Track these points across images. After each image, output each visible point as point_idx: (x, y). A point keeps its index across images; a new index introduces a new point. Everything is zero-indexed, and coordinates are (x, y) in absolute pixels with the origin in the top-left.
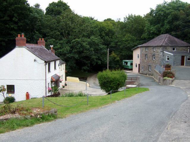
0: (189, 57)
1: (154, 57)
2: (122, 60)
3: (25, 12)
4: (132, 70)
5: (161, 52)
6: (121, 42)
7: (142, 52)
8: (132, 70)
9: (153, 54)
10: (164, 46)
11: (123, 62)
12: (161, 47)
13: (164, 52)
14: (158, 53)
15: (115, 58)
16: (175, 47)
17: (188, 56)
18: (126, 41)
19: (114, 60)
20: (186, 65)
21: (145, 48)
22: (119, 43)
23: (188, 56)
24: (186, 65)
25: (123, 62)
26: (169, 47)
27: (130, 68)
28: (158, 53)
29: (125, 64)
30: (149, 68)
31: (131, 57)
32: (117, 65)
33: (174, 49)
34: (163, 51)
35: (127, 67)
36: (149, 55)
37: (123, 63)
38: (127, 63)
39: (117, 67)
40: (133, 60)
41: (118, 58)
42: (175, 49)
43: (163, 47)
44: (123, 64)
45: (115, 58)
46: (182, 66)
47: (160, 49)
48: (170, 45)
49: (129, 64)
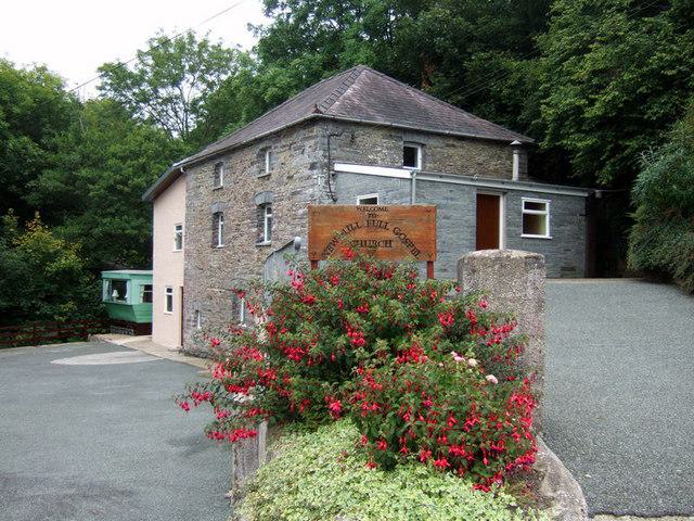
0: (529, 205)
1: (269, 219)
2: (96, 270)
3: (564, 472)
4: (145, 329)
5: (313, 167)
6: (97, 163)
7: (197, 203)
8: (145, 329)
9: (260, 200)
10: (334, 121)
11: (106, 285)
12: (317, 130)
13: (338, 167)
14: (291, 187)
15: (52, 257)
16: (417, 139)
17: (525, 199)
18: (124, 159)
19: (39, 268)
20: (509, 246)
21: (209, 169)
22: (84, 172)
23: (525, 199)
24: (509, 246)
25: (106, 285)
26: (377, 137)
27: (140, 319)
28: (291, 187)
29: (115, 294)
30: (235, 306)
31: (142, 256)
32: (65, 302)
33: (409, 160)
34: (329, 166)
35: (123, 315)
36: (236, 211)
37: (101, 292)
38: (120, 286)
39: (61, 314)
40: (150, 267)
41: (69, 259)
42: (420, 156)
43: (331, 128)
44: (105, 297)
45: (52, 257)
46: (488, 253)
47: (308, 144)
48: (381, 121)
49: (134, 296)
